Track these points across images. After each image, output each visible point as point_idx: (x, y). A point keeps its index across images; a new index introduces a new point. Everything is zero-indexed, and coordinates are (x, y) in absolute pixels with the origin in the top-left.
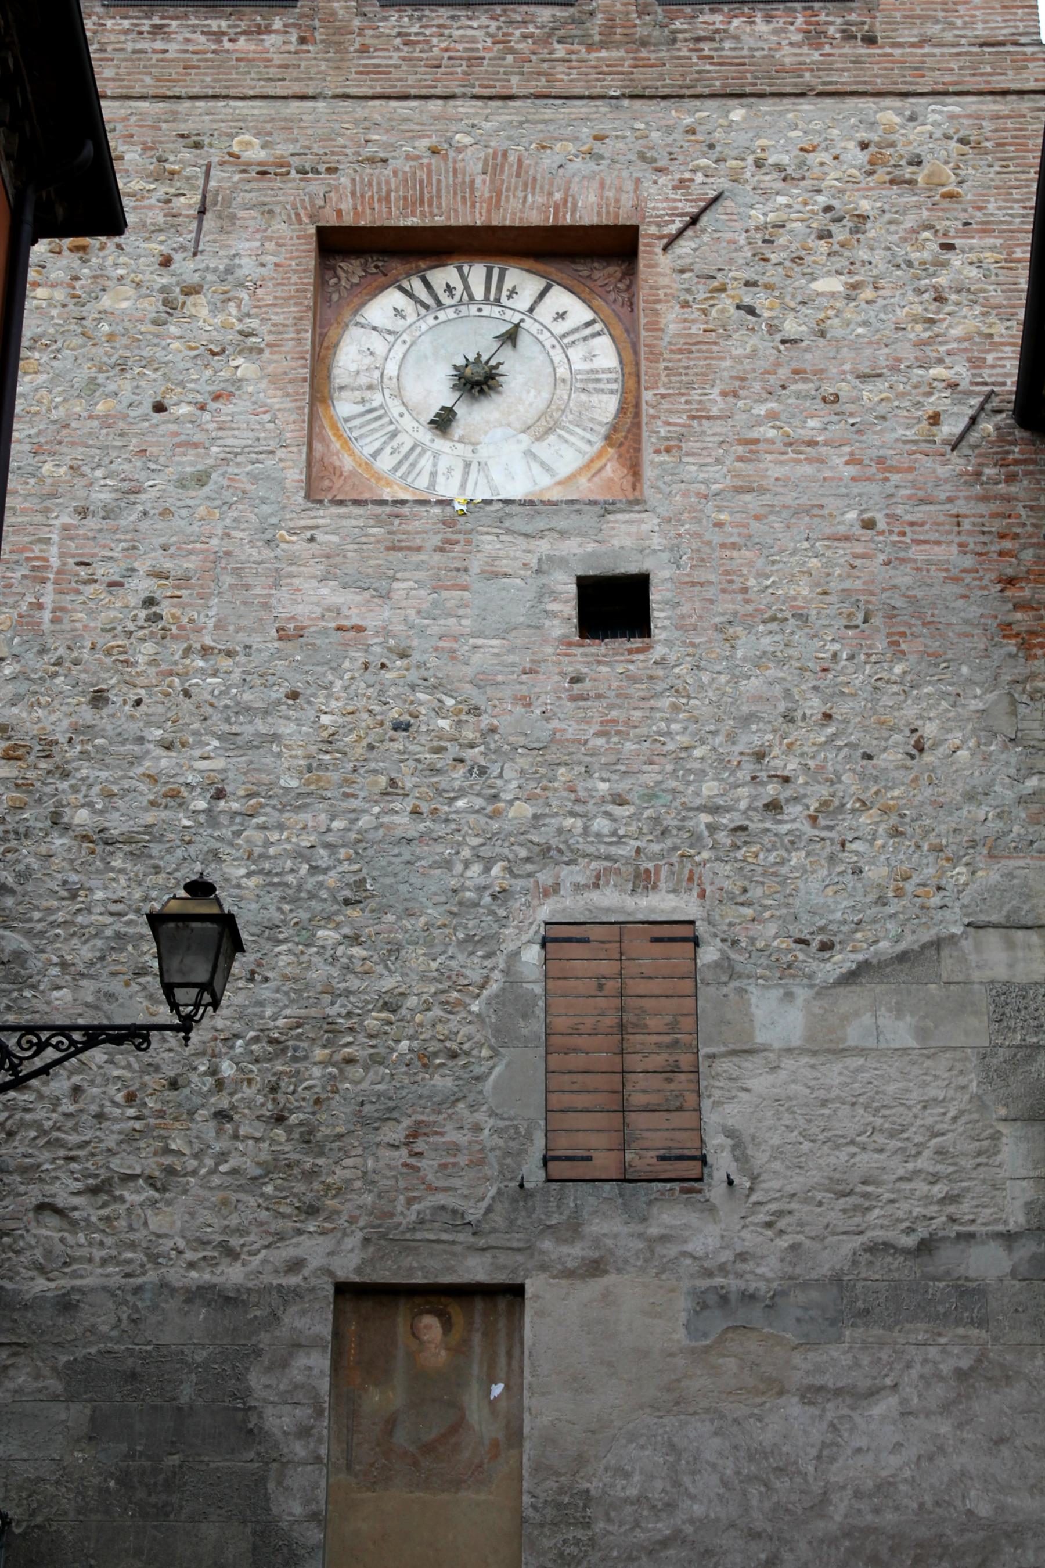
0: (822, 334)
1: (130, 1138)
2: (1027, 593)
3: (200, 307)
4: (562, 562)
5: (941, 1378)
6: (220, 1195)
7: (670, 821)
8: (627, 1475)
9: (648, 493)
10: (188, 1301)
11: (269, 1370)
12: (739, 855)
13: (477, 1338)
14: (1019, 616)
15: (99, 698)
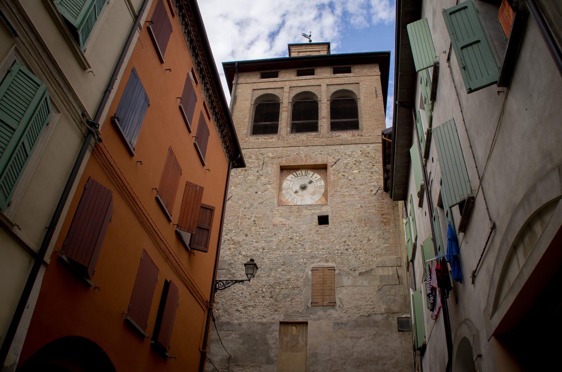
1: (250, 300)
3: (262, 178)
4: (315, 214)
7: (331, 252)
9: (328, 203)
15: (246, 235)
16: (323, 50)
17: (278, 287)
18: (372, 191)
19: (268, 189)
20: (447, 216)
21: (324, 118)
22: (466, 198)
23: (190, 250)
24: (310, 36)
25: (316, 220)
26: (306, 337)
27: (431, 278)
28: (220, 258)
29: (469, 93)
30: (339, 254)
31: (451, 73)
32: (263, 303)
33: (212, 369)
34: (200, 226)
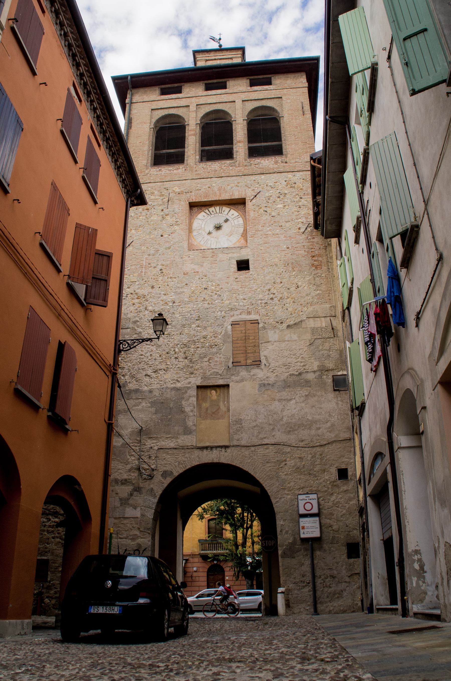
0: (279, 215)
1: (160, 363)
2: (317, 258)
3: (168, 218)
4: (234, 258)
5: (303, 396)
6: (176, 371)
7: (253, 302)
8: (248, 416)
9: (248, 245)
10: (171, 390)
11: (185, 401)
12: (266, 308)
13: (222, 394)
14: (315, 263)
15: (153, 287)
16: (236, 58)
17: (193, 346)
18: (299, 229)
19: (175, 231)
20: (387, 250)
21: (240, 142)
22: (409, 227)
23: (86, 304)
24: (220, 39)
25: (235, 266)
26: (228, 402)
27: (369, 323)
28: (123, 316)
29: (412, 95)
30: (263, 305)
31: (392, 74)
32: (176, 365)
33: (121, 443)
34: (95, 276)
